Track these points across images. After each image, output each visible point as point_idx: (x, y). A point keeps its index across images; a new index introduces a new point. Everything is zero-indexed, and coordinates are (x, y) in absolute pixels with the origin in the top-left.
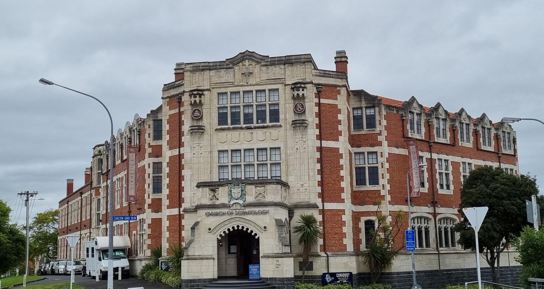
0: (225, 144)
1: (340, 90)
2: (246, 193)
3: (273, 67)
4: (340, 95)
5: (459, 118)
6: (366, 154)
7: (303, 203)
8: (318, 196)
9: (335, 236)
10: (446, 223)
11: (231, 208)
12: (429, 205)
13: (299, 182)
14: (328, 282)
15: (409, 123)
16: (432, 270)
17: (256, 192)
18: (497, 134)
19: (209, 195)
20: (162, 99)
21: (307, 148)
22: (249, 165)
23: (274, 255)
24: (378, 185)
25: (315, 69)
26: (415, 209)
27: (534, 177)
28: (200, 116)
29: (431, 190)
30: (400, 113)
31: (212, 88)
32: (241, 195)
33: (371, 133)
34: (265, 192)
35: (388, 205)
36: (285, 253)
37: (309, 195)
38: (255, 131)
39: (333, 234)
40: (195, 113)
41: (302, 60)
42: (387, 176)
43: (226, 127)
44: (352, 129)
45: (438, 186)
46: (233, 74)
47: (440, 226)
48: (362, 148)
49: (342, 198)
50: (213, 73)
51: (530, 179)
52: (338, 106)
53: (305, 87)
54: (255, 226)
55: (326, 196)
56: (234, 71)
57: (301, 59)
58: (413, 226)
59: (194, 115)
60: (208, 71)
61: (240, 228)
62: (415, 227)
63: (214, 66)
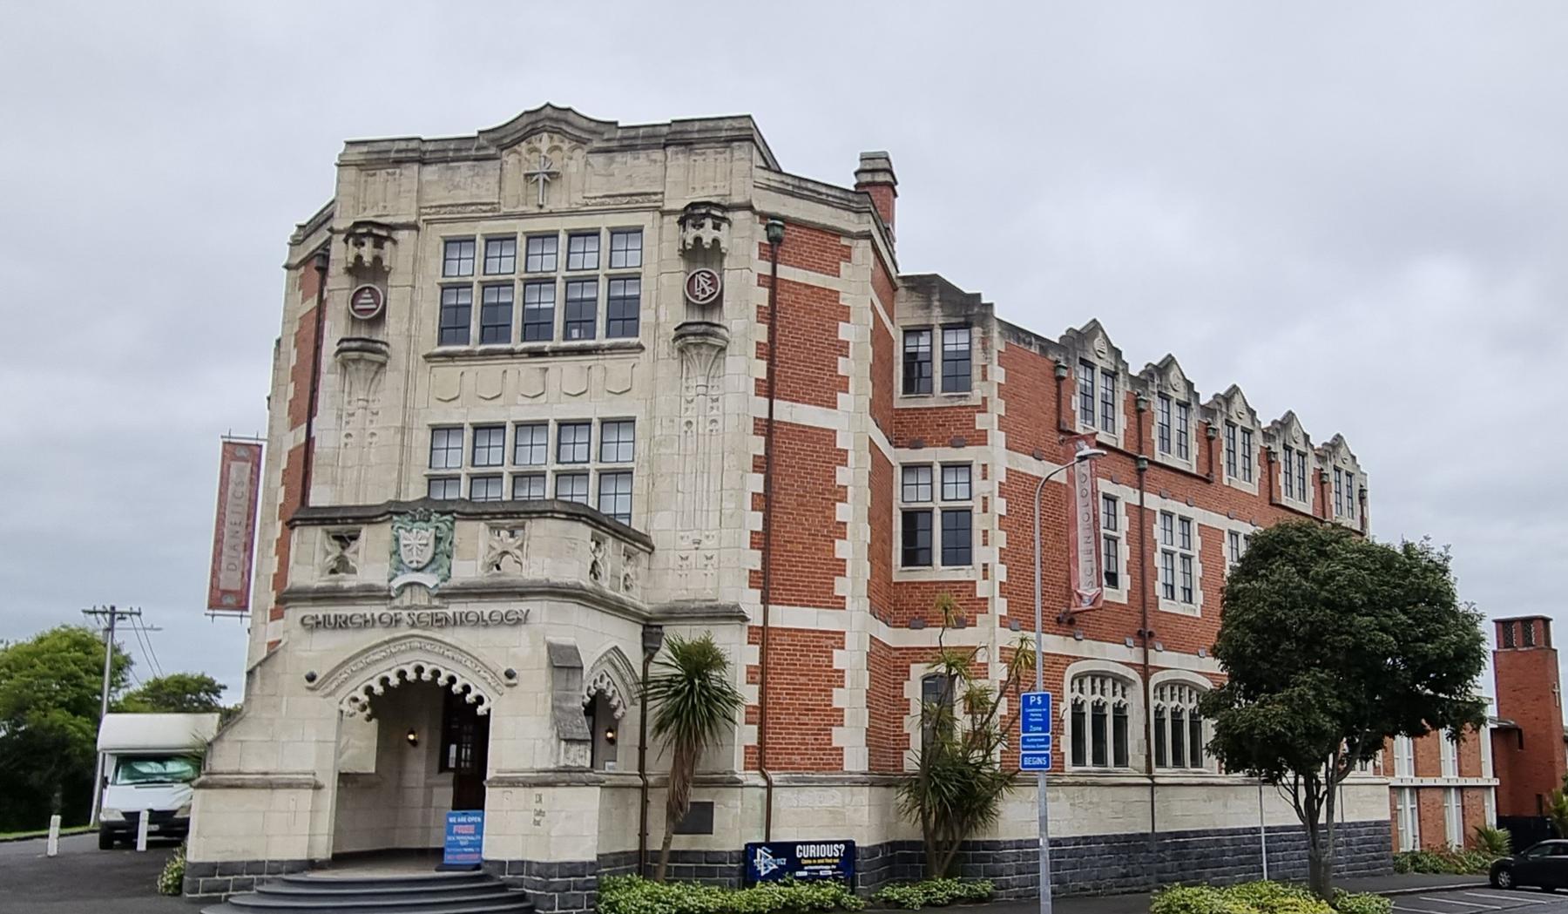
0: (454, 403)
1: (850, 247)
2: (455, 549)
3: (628, 157)
4: (850, 262)
5: (1224, 410)
6: (937, 468)
7: (697, 604)
8: (750, 582)
9: (805, 719)
10: (1177, 697)
11: (397, 602)
12: (1130, 642)
13: (688, 533)
14: (763, 874)
15: (1078, 394)
16: (1129, 833)
17: (490, 546)
18: (1322, 469)
19: (323, 556)
20: (285, 271)
21: (720, 423)
22: (530, 477)
23: (535, 775)
24: (970, 567)
25: (768, 168)
26: (1086, 647)
27: (1443, 550)
28: (374, 310)
29: (1138, 597)
30: (1050, 357)
31: (424, 221)
32: (435, 554)
33: (956, 404)
34: (522, 545)
35: (998, 629)
36: (567, 770)
37: (719, 577)
38: (554, 364)
39: (797, 709)
40: (361, 301)
41: (724, 134)
42: (1000, 539)
43: (463, 348)
44: (898, 392)
45: (1159, 590)
46: (498, 177)
47: (1159, 705)
48: (924, 449)
49: (836, 594)
50: (430, 172)
51: (1430, 556)
52: (842, 296)
53: (724, 219)
54: (477, 669)
55: (778, 584)
56: (501, 169)
57: (720, 130)
58: (1076, 700)
59: (357, 307)
60: (416, 167)
61: (426, 676)
62: (1085, 705)
63: (439, 151)
